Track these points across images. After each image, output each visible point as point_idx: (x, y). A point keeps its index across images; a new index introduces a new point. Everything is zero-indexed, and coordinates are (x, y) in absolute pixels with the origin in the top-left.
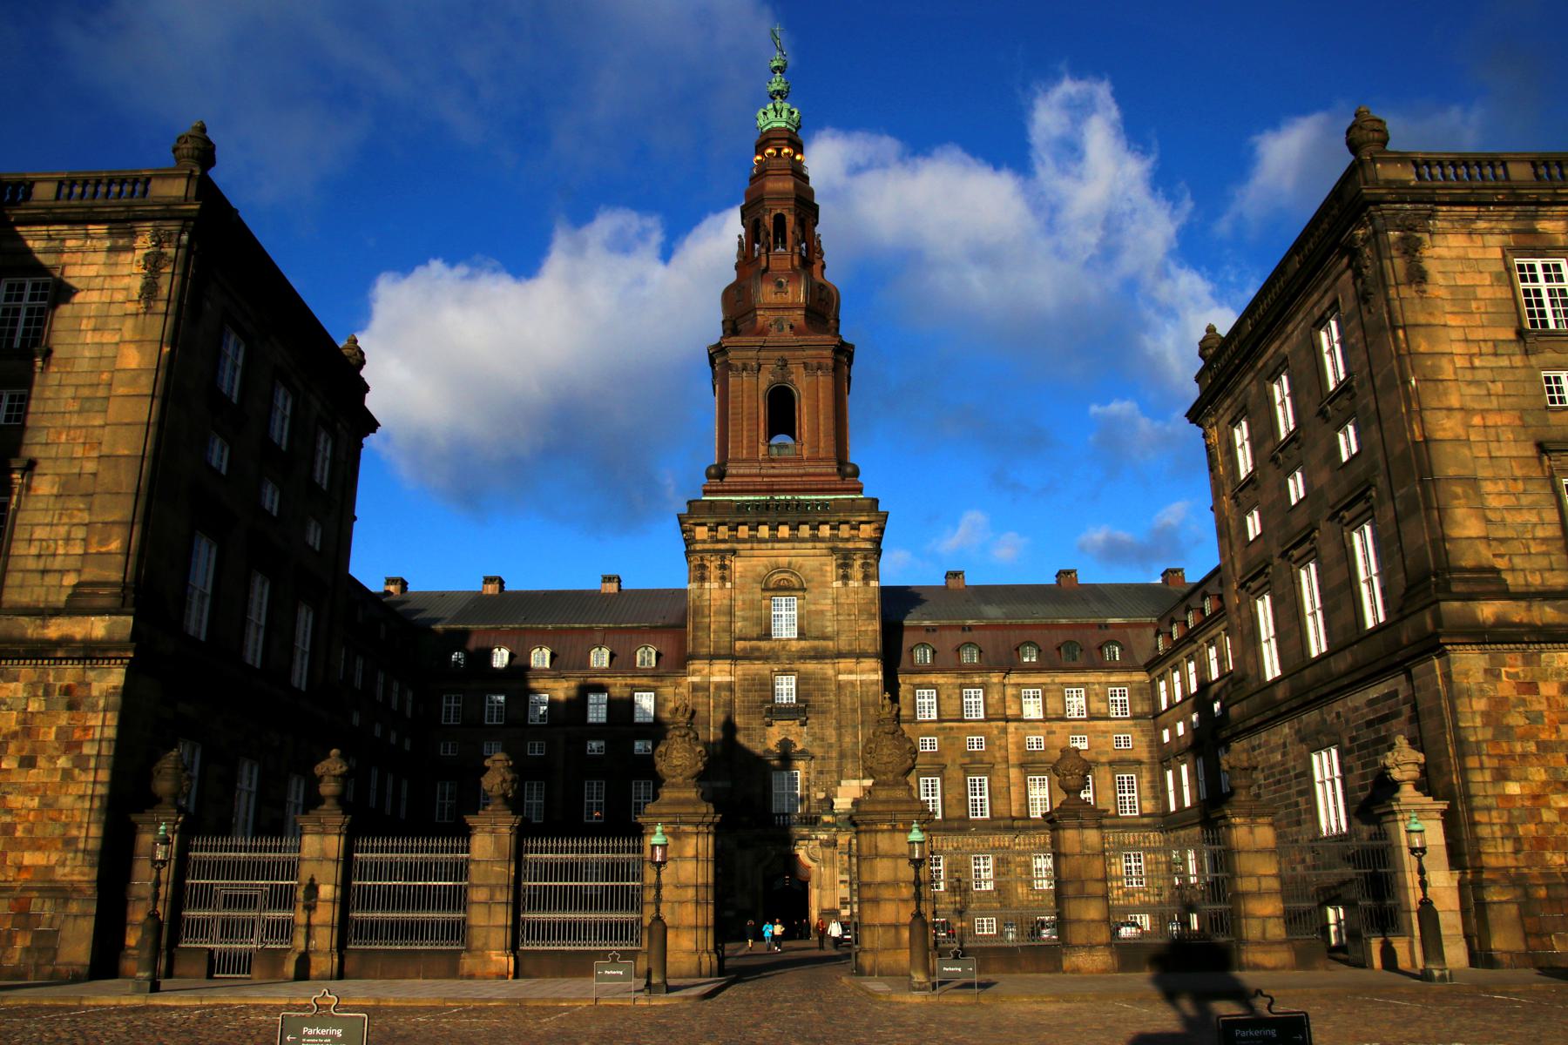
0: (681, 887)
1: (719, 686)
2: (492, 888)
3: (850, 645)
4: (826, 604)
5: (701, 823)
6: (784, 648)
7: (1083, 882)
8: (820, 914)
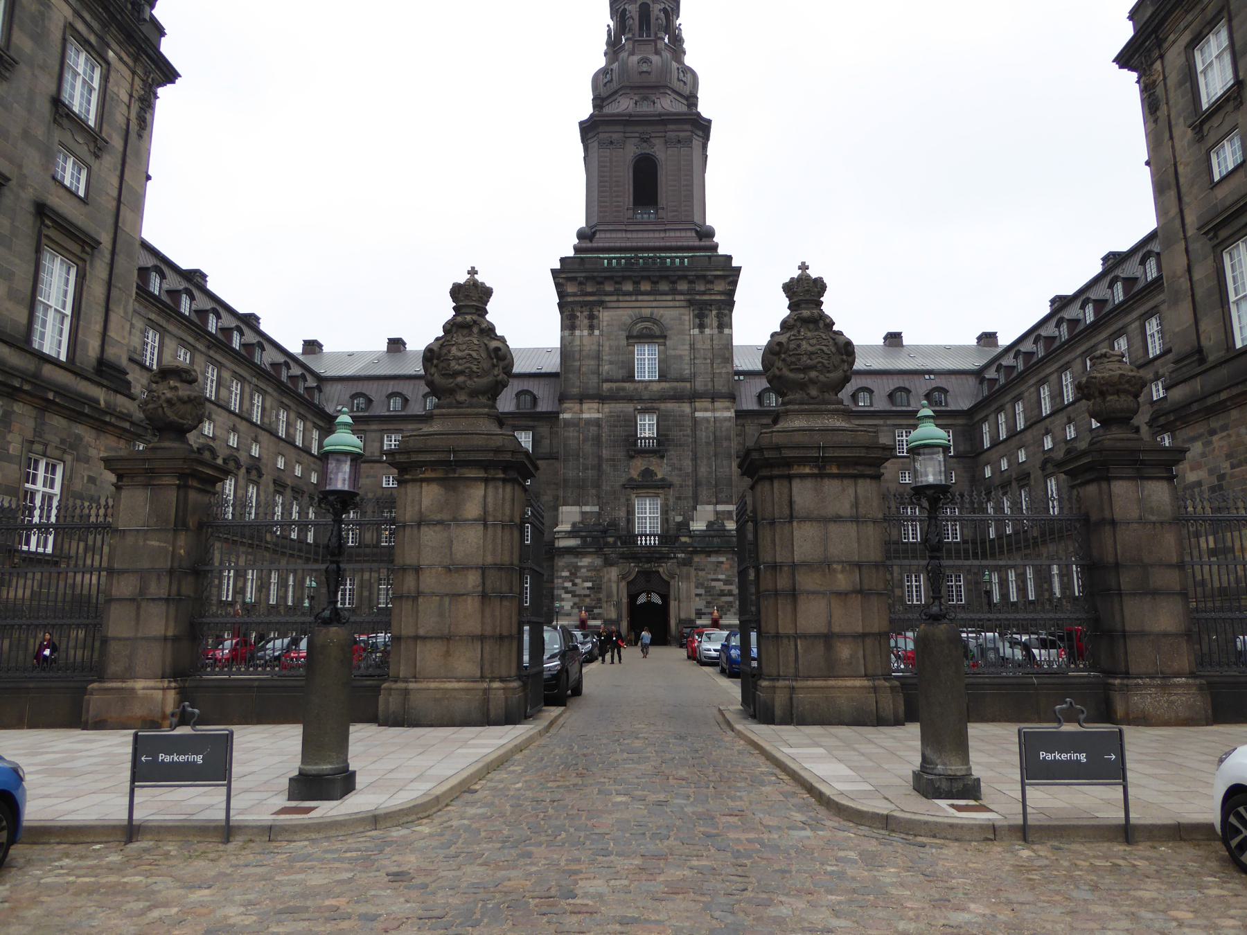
0: (457, 570)
2: (143, 574)
3: (706, 385)
4: (684, 350)
6: (646, 388)
8: (677, 625)
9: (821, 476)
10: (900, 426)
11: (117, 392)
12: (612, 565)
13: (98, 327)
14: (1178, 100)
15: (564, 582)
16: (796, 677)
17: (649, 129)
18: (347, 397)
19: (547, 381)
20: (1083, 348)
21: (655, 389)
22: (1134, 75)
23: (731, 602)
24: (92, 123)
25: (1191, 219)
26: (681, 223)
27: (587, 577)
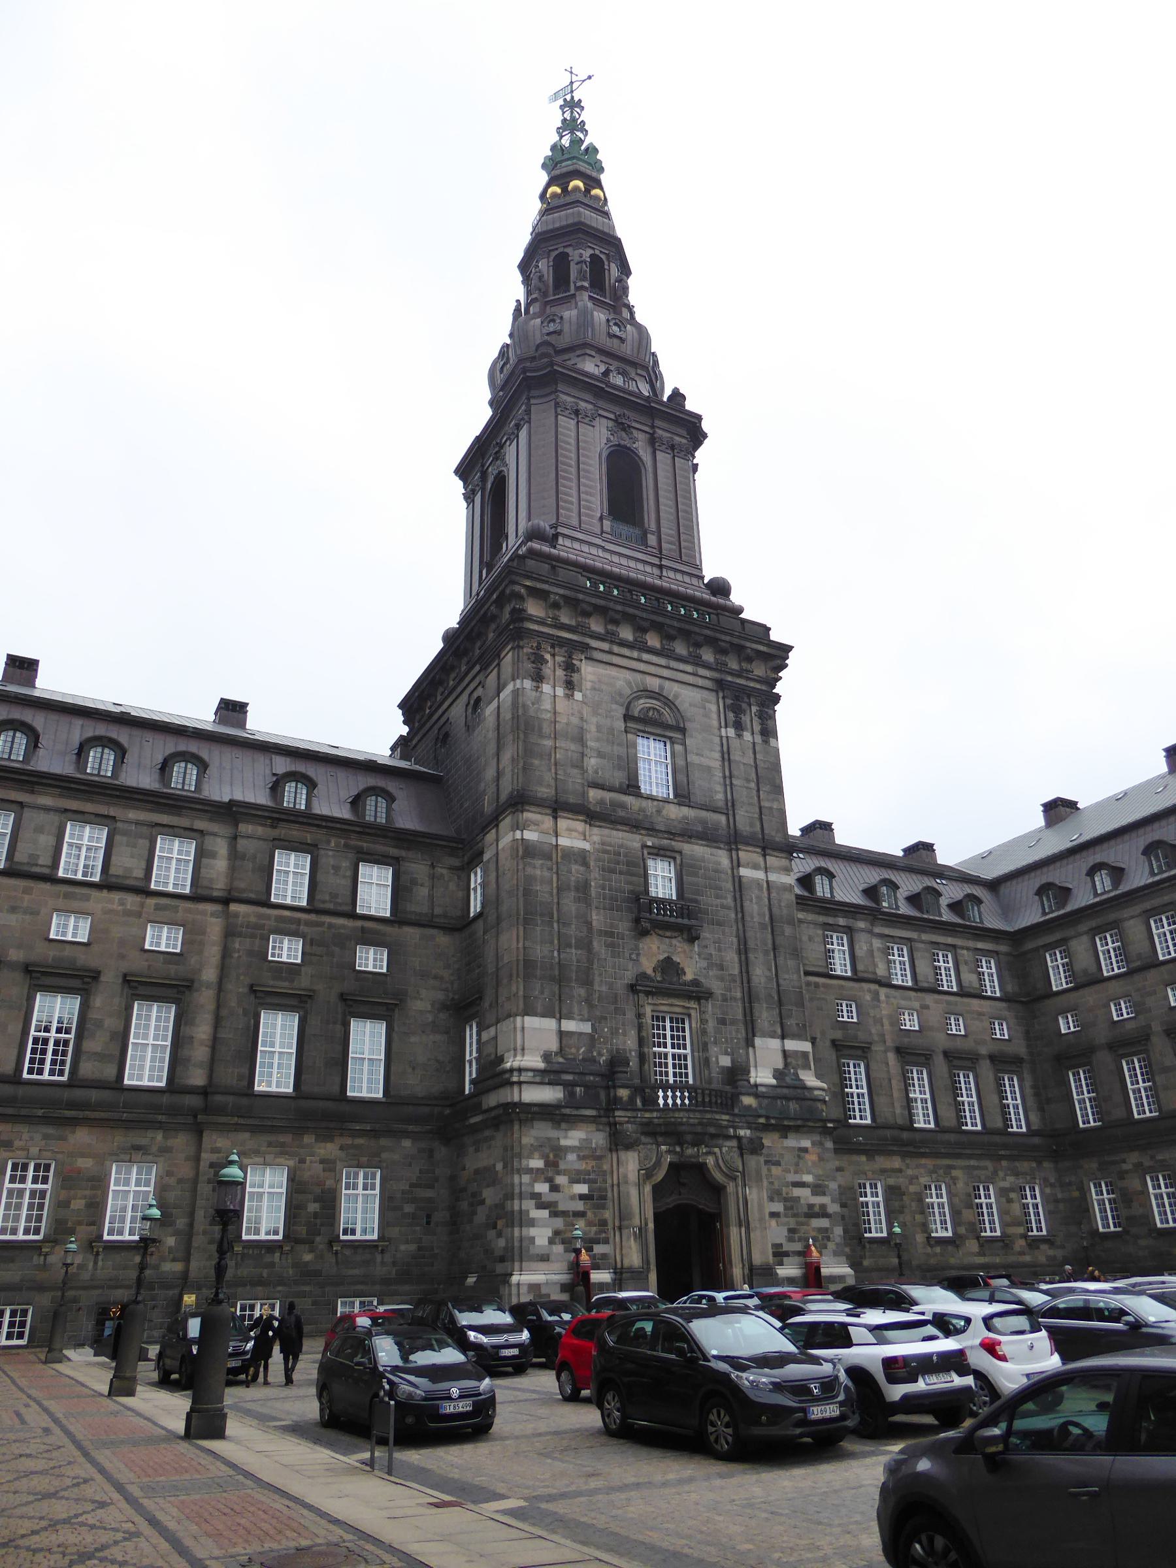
1: (571, 855)
12: (628, 1147)
15: (535, 1181)
21: (673, 816)
23: (826, 1230)
27: (578, 1172)
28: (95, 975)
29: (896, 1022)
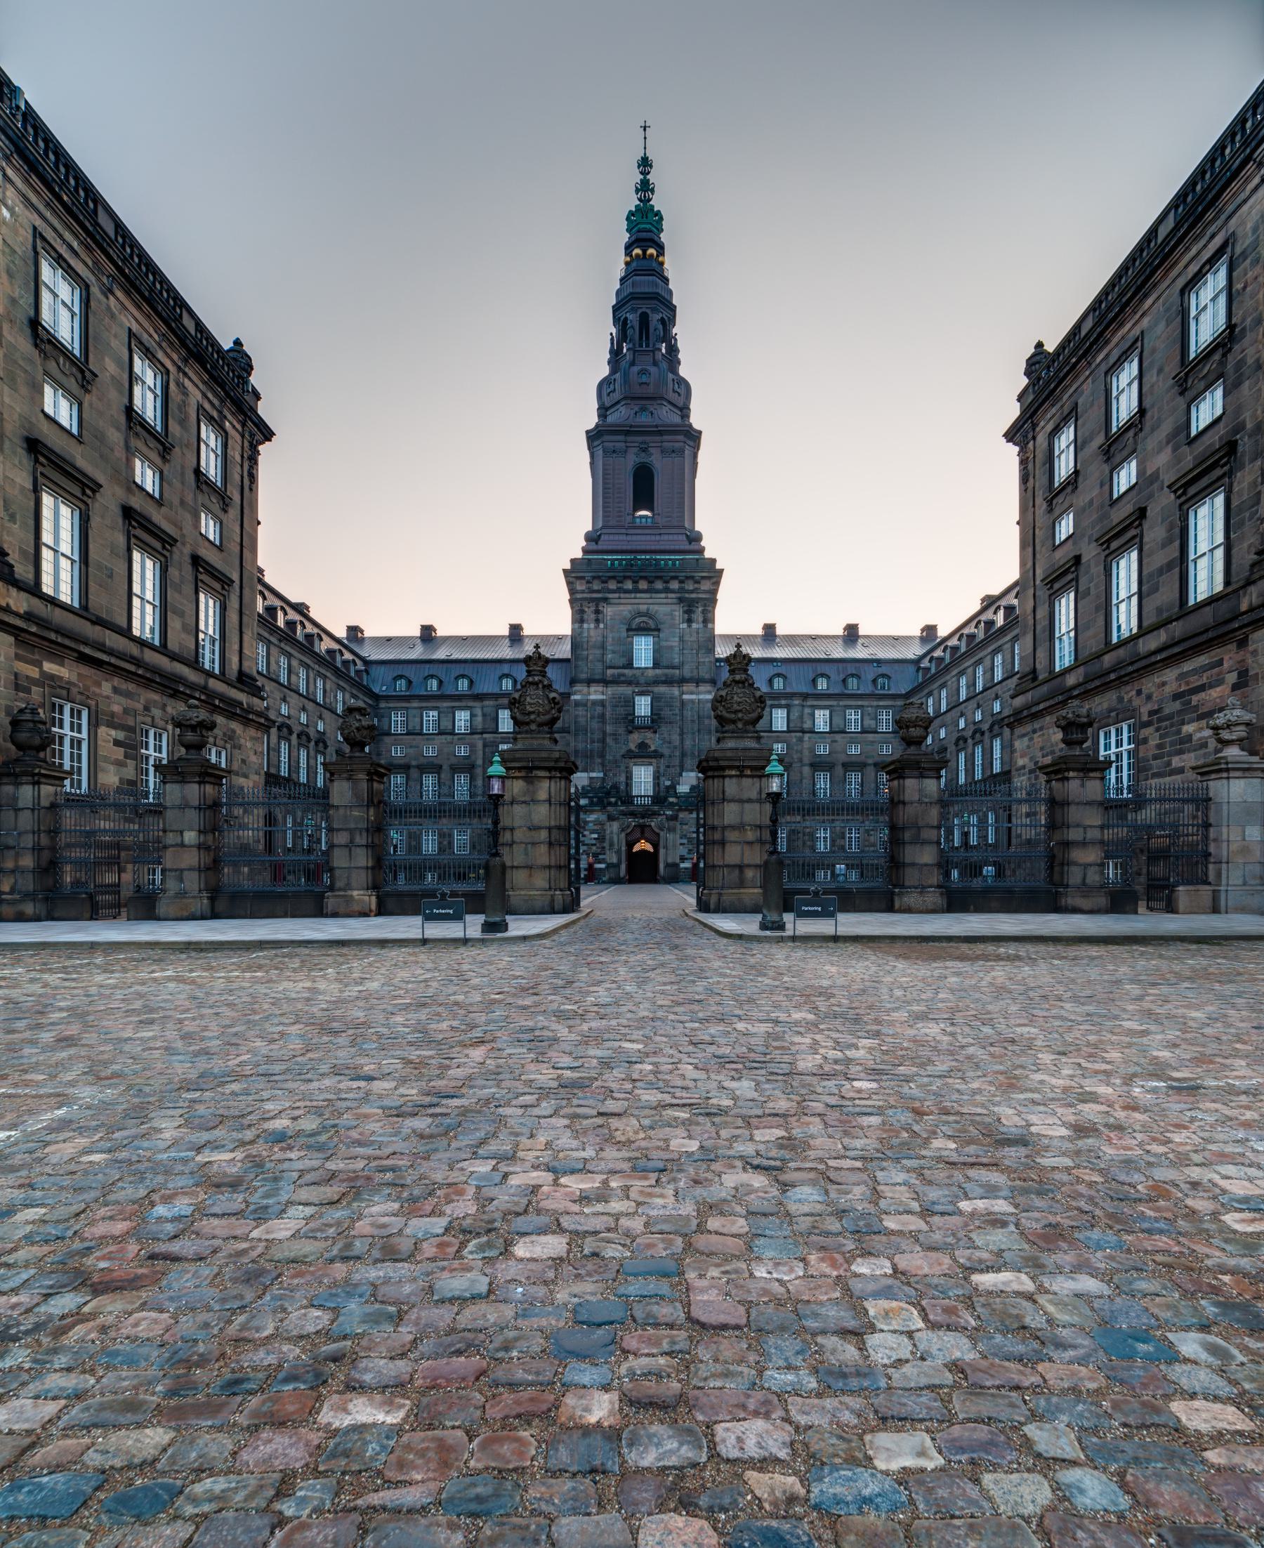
1: (595, 703)
2: (351, 831)
4: (674, 642)
5: (555, 769)
7: (919, 828)
9: (741, 776)
10: (850, 707)
11: (254, 695)
13: (236, 647)
14: (1042, 480)
16: (722, 888)
17: (648, 439)
18: (390, 678)
19: (560, 665)
20: (992, 647)
22: (1017, 449)
24: (77, 352)
25: (1038, 571)
26: (674, 527)
28: (441, 767)
29: (812, 750)
